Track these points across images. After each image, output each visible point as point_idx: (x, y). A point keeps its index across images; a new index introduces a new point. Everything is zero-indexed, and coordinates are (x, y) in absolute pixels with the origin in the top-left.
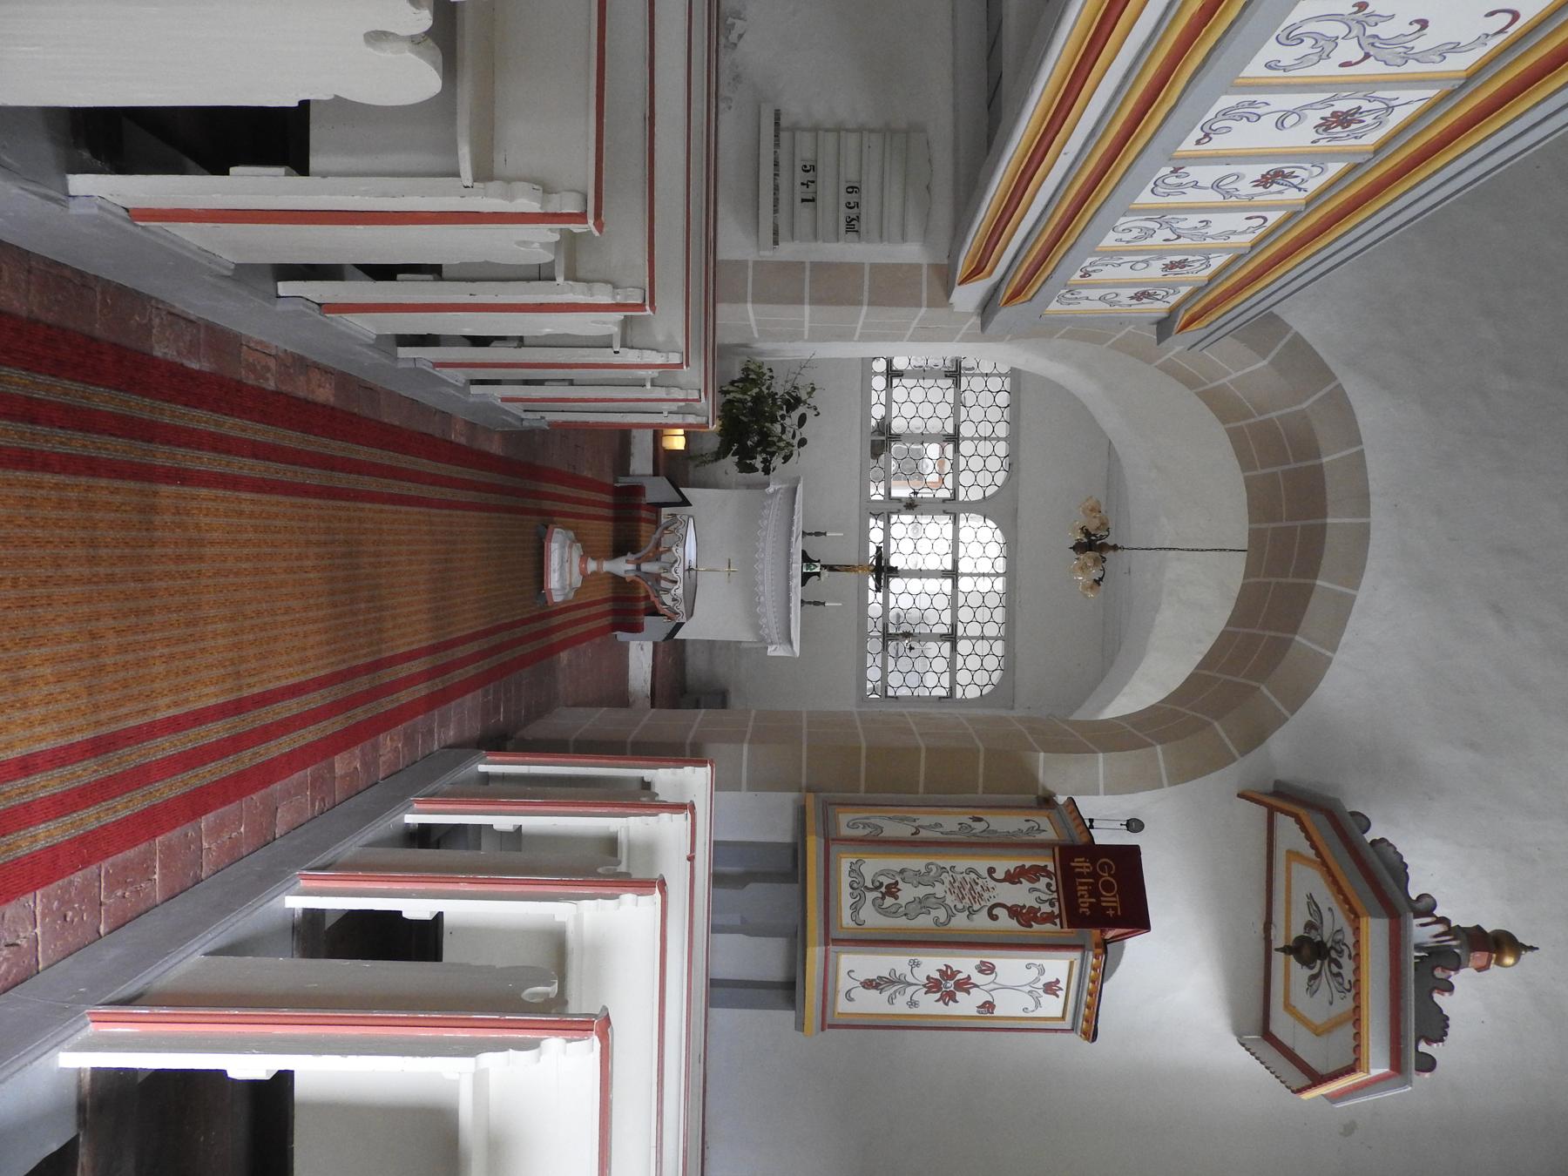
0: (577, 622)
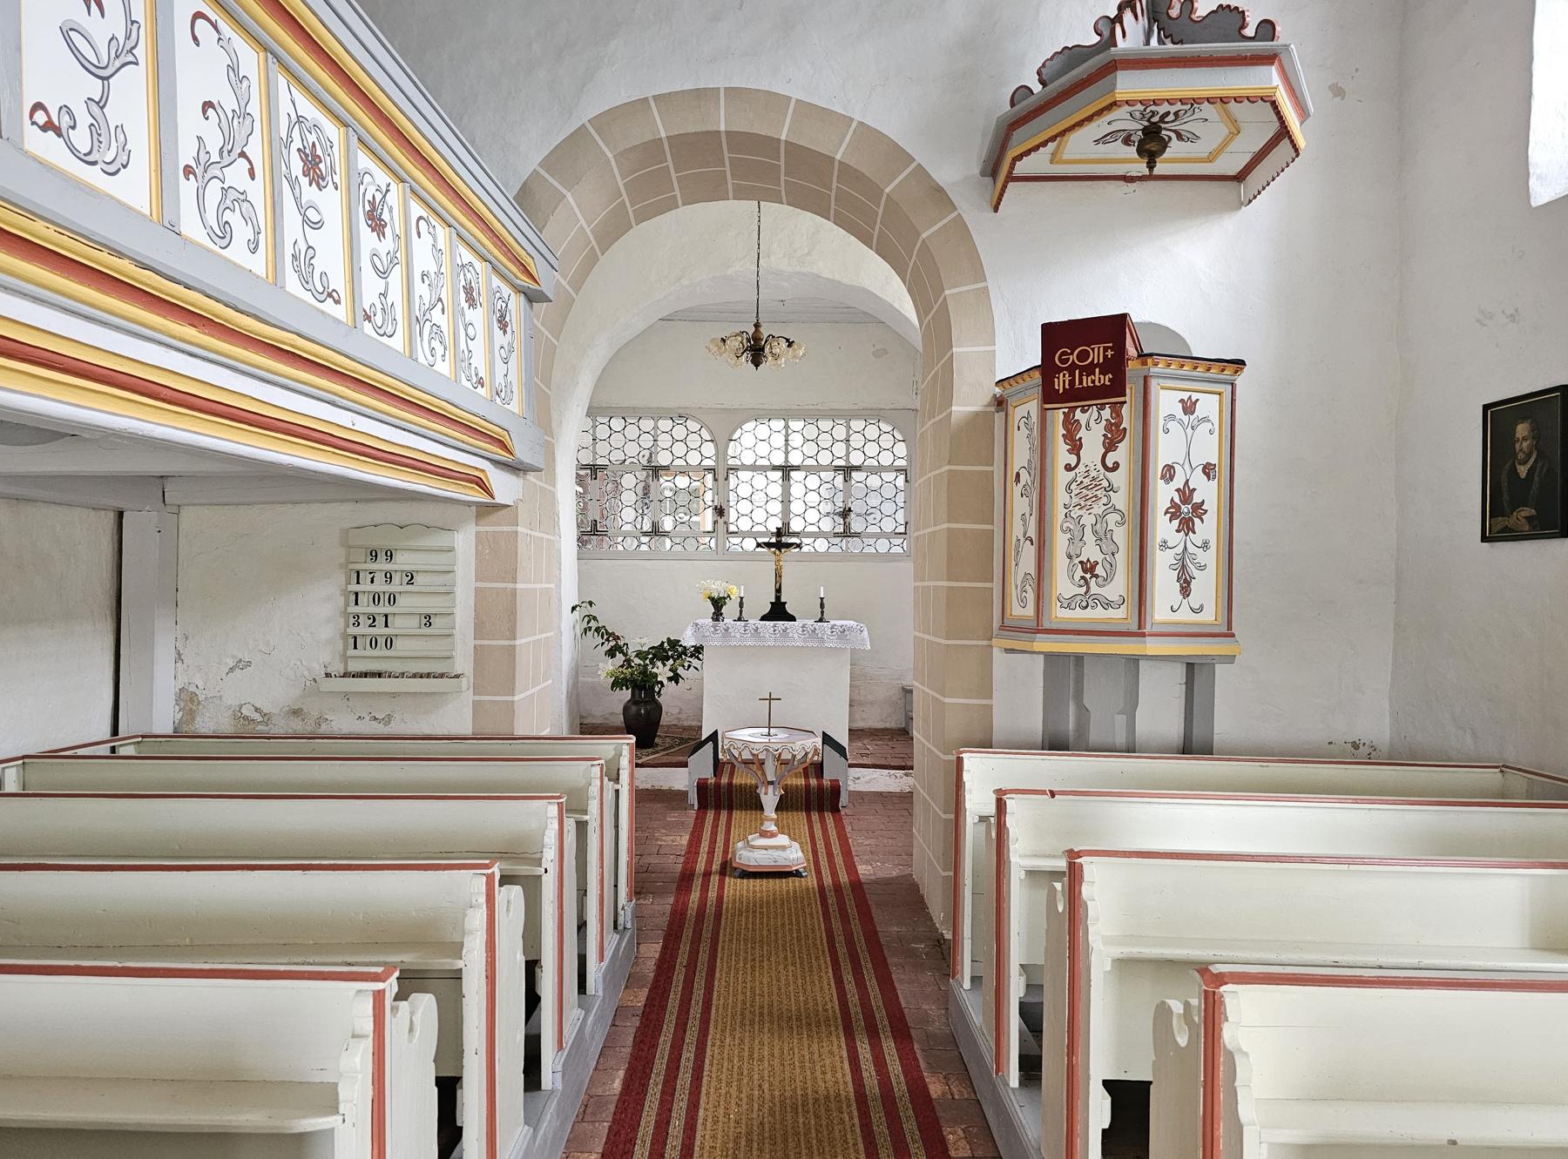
0: (830, 855)
